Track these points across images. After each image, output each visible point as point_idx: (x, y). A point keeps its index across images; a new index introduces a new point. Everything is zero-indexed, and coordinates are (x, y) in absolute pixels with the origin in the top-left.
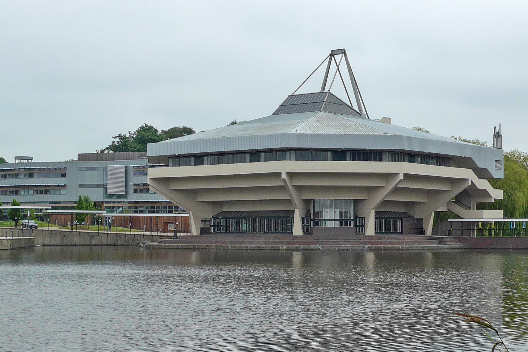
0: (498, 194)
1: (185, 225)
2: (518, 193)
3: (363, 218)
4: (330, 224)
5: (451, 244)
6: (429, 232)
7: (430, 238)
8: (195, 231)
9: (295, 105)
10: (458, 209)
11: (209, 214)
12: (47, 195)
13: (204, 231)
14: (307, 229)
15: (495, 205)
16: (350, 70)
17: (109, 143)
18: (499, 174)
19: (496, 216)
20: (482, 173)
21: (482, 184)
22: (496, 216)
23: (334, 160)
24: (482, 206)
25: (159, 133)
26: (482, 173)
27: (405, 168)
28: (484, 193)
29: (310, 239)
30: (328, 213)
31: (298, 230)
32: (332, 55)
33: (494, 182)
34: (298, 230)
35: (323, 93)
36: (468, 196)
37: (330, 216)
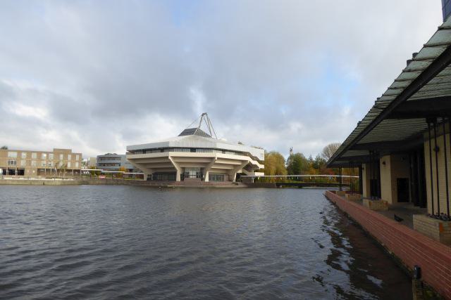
0: (261, 166)
1: (142, 176)
2: (390, 202)
3: (54, 149)
4: (191, 177)
5: (240, 185)
6: (234, 181)
7: (234, 183)
8: (145, 179)
10: (246, 172)
11: (151, 173)
12: (279, 189)
13: (148, 179)
14: (182, 178)
15: (261, 171)
18: (262, 159)
19: (262, 174)
20: (253, 158)
22: (262, 174)
24: (257, 171)
26: (253, 158)
28: (256, 166)
29: (182, 182)
30: (191, 173)
31: (178, 178)
32: (203, 115)
33: (261, 162)
34: (178, 178)
36: (249, 167)
37: (193, 174)
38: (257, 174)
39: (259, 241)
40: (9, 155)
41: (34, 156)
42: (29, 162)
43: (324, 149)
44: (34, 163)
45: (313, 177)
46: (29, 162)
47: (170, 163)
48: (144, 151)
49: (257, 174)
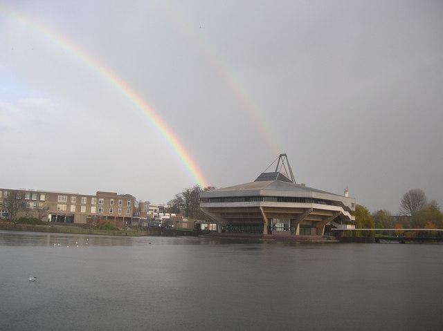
0: (353, 218)
4: (278, 230)
9: (264, 177)
10: (336, 225)
14: (270, 232)
15: (352, 223)
16: (290, 168)
17: (181, 192)
18: (353, 209)
20: (346, 209)
21: (346, 214)
23: (23, 193)
25: (371, 214)
26: (346, 209)
27: (315, 206)
31: (265, 232)
32: (280, 156)
33: (351, 213)
34: (265, 232)
35: (276, 173)
36: (340, 218)
38: (349, 227)
39: (146, 221)
40: (84, 211)
41: (84, 201)
42: (78, 208)
43: (403, 202)
44: (83, 210)
45: (438, 231)
46: (78, 208)
47: (260, 213)
48: (222, 199)
49: (349, 227)
